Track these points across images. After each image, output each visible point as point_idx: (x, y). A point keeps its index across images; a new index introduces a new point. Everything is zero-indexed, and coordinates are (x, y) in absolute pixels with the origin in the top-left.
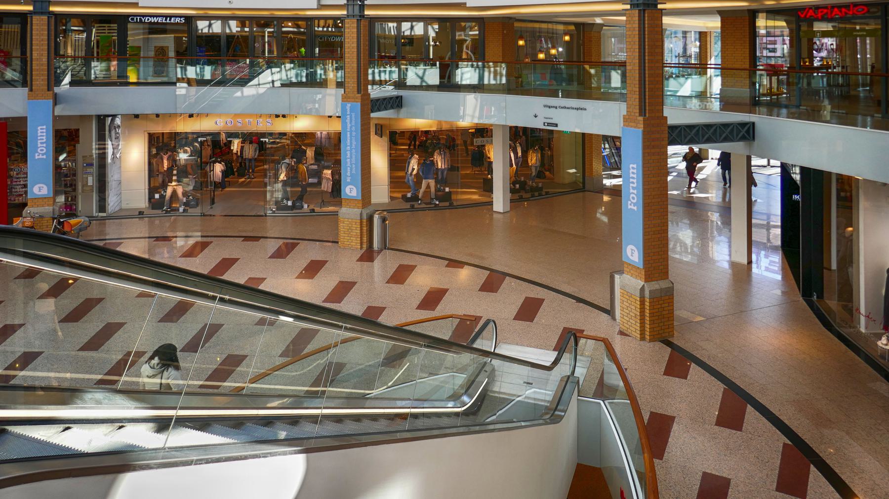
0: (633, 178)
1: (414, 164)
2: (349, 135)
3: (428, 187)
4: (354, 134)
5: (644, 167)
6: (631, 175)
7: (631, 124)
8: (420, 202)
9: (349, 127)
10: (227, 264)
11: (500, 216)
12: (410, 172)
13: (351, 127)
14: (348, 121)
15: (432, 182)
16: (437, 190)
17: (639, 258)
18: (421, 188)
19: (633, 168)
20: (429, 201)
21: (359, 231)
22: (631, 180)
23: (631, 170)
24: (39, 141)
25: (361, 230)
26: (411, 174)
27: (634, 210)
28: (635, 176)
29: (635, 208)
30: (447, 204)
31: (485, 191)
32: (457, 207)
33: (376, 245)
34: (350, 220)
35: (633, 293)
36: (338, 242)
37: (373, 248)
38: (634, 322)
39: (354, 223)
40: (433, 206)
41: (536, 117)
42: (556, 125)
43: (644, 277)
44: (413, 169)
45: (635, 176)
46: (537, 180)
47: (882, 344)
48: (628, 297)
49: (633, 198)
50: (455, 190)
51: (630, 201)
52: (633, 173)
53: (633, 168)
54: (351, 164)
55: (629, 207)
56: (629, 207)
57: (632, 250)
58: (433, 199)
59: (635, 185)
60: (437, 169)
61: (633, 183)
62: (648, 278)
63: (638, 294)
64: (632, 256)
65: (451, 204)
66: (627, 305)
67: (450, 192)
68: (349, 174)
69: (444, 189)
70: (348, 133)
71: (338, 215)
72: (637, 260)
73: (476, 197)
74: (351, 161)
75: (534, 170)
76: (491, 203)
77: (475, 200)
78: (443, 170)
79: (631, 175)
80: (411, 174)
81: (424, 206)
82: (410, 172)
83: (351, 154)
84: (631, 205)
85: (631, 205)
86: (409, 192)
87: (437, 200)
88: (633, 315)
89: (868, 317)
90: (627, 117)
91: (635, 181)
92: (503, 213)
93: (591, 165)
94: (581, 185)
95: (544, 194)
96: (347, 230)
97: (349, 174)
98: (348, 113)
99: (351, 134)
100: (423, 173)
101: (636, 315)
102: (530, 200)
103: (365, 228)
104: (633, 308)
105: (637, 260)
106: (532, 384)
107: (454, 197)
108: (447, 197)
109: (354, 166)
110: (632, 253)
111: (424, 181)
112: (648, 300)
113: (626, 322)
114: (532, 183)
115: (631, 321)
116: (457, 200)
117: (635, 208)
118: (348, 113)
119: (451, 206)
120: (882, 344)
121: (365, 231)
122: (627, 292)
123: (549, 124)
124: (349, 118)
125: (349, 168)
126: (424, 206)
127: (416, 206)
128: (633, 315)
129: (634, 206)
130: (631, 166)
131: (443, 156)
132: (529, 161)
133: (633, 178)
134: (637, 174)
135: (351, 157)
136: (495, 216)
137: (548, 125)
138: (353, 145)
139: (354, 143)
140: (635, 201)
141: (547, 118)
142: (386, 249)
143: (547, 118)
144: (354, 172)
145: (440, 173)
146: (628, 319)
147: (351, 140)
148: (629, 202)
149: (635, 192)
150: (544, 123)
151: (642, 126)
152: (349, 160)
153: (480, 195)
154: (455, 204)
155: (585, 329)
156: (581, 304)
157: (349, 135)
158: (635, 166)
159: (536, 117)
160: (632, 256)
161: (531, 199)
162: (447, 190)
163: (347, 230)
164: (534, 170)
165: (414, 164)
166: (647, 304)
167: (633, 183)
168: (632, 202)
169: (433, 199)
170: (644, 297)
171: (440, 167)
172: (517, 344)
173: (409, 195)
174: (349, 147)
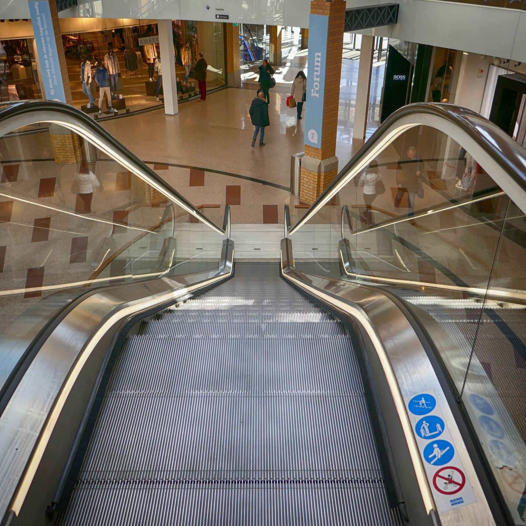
0: (317, 66)
1: (88, 71)
2: (43, 42)
3: (105, 95)
4: (48, 39)
5: (328, 55)
6: (316, 64)
7: (318, 10)
8: (100, 112)
9: (41, 31)
10: (314, 134)
11: (172, 118)
12: (86, 80)
13: (44, 31)
14: (39, 23)
15: (108, 89)
16: (113, 98)
17: (318, 141)
18: (99, 97)
19: (318, 57)
20: (107, 110)
21: (72, 146)
22: (316, 68)
23: (316, 59)
24: (316, 73)
25: (74, 144)
26: (87, 83)
27: (317, 97)
28: (319, 64)
29: (318, 95)
30: (124, 111)
31: (148, 95)
32: (133, 114)
33: (88, 158)
34: (62, 136)
35: (312, 170)
36: (53, 160)
37: (87, 161)
38: (312, 193)
39: (66, 139)
40: (113, 114)
41: (208, 9)
42: (227, 17)
43: (321, 156)
44: (89, 77)
45: (319, 64)
46: (190, 80)
47: (458, 186)
48: (308, 174)
49: (316, 86)
50: (130, 96)
51: (313, 88)
52: (318, 61)
53: (318, 57)
54: (52, 75)
55: (313, 95)
56: (313, 95)
57: (312, 134)
58: (110, 108)
59: (318, 74)
60: (110, 75)
61: (317, 71)
62: (324, 157)
63: (317, 171)
64: (312, 139)
65: (128, 111)
66: (307, 180)
67: (123, 100)
68: (51, 86)
69: (118, 97)
70: (42, 38)
71: (49, 131)
72: (316, 142)
73: (143, 102)
74: (51, 72)
75: (187, 69)
76: (162, 106)
77: (144, 105)
78: (114, 76)
79: (316, 64)
80: (87, 83)
81: (104, 115)
82: (86, 80)
83: (49, 63)
84: (314, 92)
85: (314, 92)
86: (88, 102)
87: (114, 108)
88: (312, 188)
89: (454, 167)
90: (315, 3)
91: (319, 69)
92: (175, 115)
93: (232, 60)
94: (224, 82)
95: (193, 95)
96: (61, 146)
97: (51, 86)
98: (38, 14)
99: (45, 40)
100: (98, 81)
101: (314, 187)
102: (188, 101)
103: (77, 142)
104: (312, 182)
105: (316, 142)
106: (260, 249)
107: (128, 104)
108: (121, 104)
109: (55, 76)
110: (313, 136)
111: (101, 89)
112: (323, 174)
113: (305, 194)
114: (186, 83)
115: (309, 192)
116: (133, 106)
117: (318, 95)
118: (38, 14)
119: (129, 113)
120: (458, 186)
121: (77, 145)
122: (308, 170)
123: (221, 17)
124: (39, 21)
125: (50, 80)
126: (104, 115)
127: (99, 117)
128: (312, 188)
129: (317, 93)
130: (316, 54)
131: (113, 61)
132: (183, 60)
133: (317, 66)
134: (321, 62)
135: (50, 68)
136: (167, 118)
137: (220, 18)
138: (50, 53)
139: (50, 50)
140: (317, 89)
141: (218, 10)
142: (97, 160)
143: (218, 10)
144: (56, 84)
145: (112, 79)
146: (307, 192)
147: (46, 46)
148: (313, 90)
149: (318, 80)
150: (216, 15)
151: (329, 12)
152: (48, 70)
153: (147, 100)
154: (131, 111)
155: (277, 204)
156: (267, 186)
157: (43, 42)
158: (320, 54)
159: (208, 9)
160: (312, 139)
161: (190, 99)
162: (121, 97)
163: (61, 146)
164: (187, 69)
165: (88, 71)
166: (322, 177)
167: (317, 71)
168: (315, 90)
169: (110, 108)
170: (320, 172)
171: (111, 73)
172: (238, 223)
173: (89, 106)
174: (46, 56)
